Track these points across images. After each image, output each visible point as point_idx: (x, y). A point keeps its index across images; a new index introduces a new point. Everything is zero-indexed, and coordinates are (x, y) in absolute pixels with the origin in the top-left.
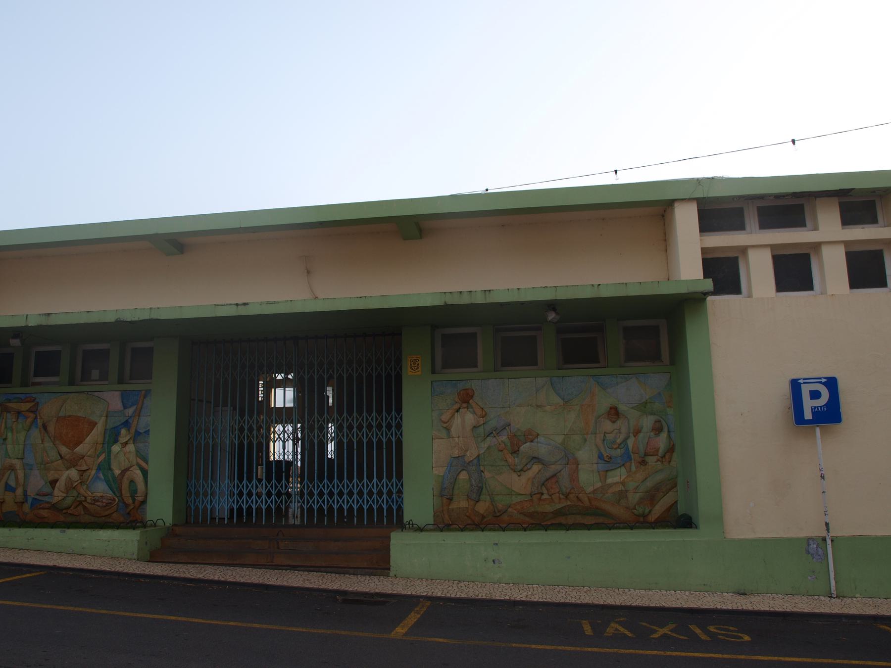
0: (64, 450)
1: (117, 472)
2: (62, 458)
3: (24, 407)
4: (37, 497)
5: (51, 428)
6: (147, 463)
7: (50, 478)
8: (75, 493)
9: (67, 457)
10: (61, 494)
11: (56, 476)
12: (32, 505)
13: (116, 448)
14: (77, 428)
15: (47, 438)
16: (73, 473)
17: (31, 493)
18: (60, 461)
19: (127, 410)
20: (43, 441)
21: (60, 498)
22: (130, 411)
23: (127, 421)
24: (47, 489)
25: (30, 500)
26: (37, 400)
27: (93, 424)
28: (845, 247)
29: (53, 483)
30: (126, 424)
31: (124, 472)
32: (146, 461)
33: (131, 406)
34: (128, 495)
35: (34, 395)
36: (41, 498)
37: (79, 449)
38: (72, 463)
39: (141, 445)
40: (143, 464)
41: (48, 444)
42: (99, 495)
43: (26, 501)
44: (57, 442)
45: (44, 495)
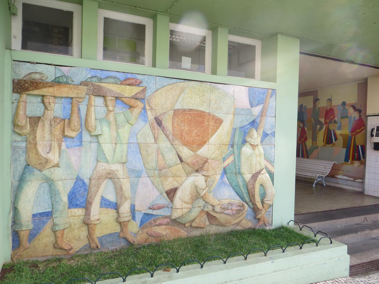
0: (186, 152)
1: (248, 177)
2: (181, 161)
3: (129, 91)
4: (151, 212)
5: (168, 123)
6: (273, 166)
7: (168, 187)
8: (201, 203)
9: (189, 161)
10: (185, 205)
11: (175, 184)
12: (142, 222)
13: (246, 150)
14: (198, 125)
15: (162, 137)
16: (199, 179)
17: (142, 208)
18: (180, 166)
19: (253, 109)
20: (156, 139)
21: (185, 210)
22: (257, 110)
23: (254, 121)
24: (164, 200)
25: (139, 217)
26: (144, 84)
27: (219, 122)
28: (181, 65)
29: (171, 193)
30: (253, 124)
31: (255, 176)
32: (271, 162)
33: (257, 105)
34: (259, 200)
35: (140, 77)
36: (155, 212)
37: (203, 151)
38: (199, 167)
39: (267, 147)
40: (270, 167)
41: (164, 144)
42: (226, 202)
43: (134, 218)
44: (177, 142)
45: (159, 208)
